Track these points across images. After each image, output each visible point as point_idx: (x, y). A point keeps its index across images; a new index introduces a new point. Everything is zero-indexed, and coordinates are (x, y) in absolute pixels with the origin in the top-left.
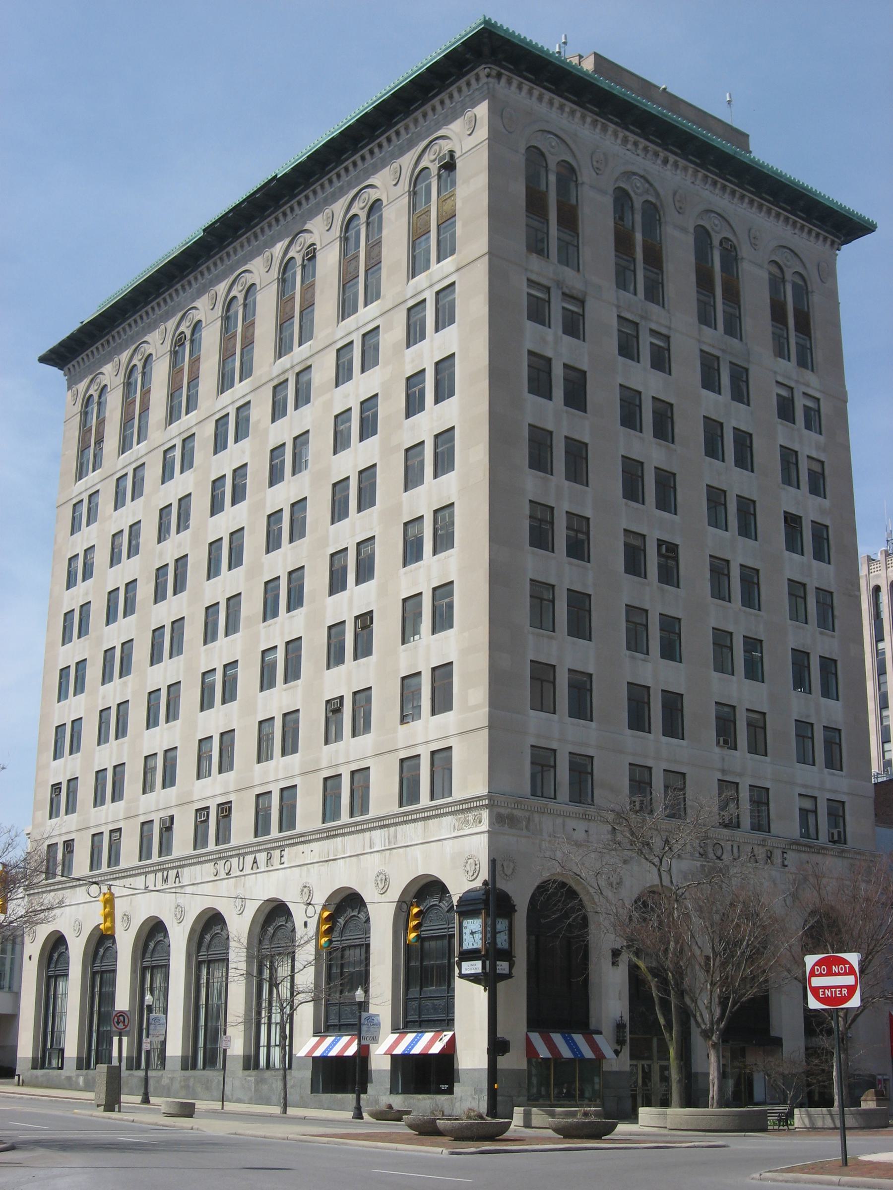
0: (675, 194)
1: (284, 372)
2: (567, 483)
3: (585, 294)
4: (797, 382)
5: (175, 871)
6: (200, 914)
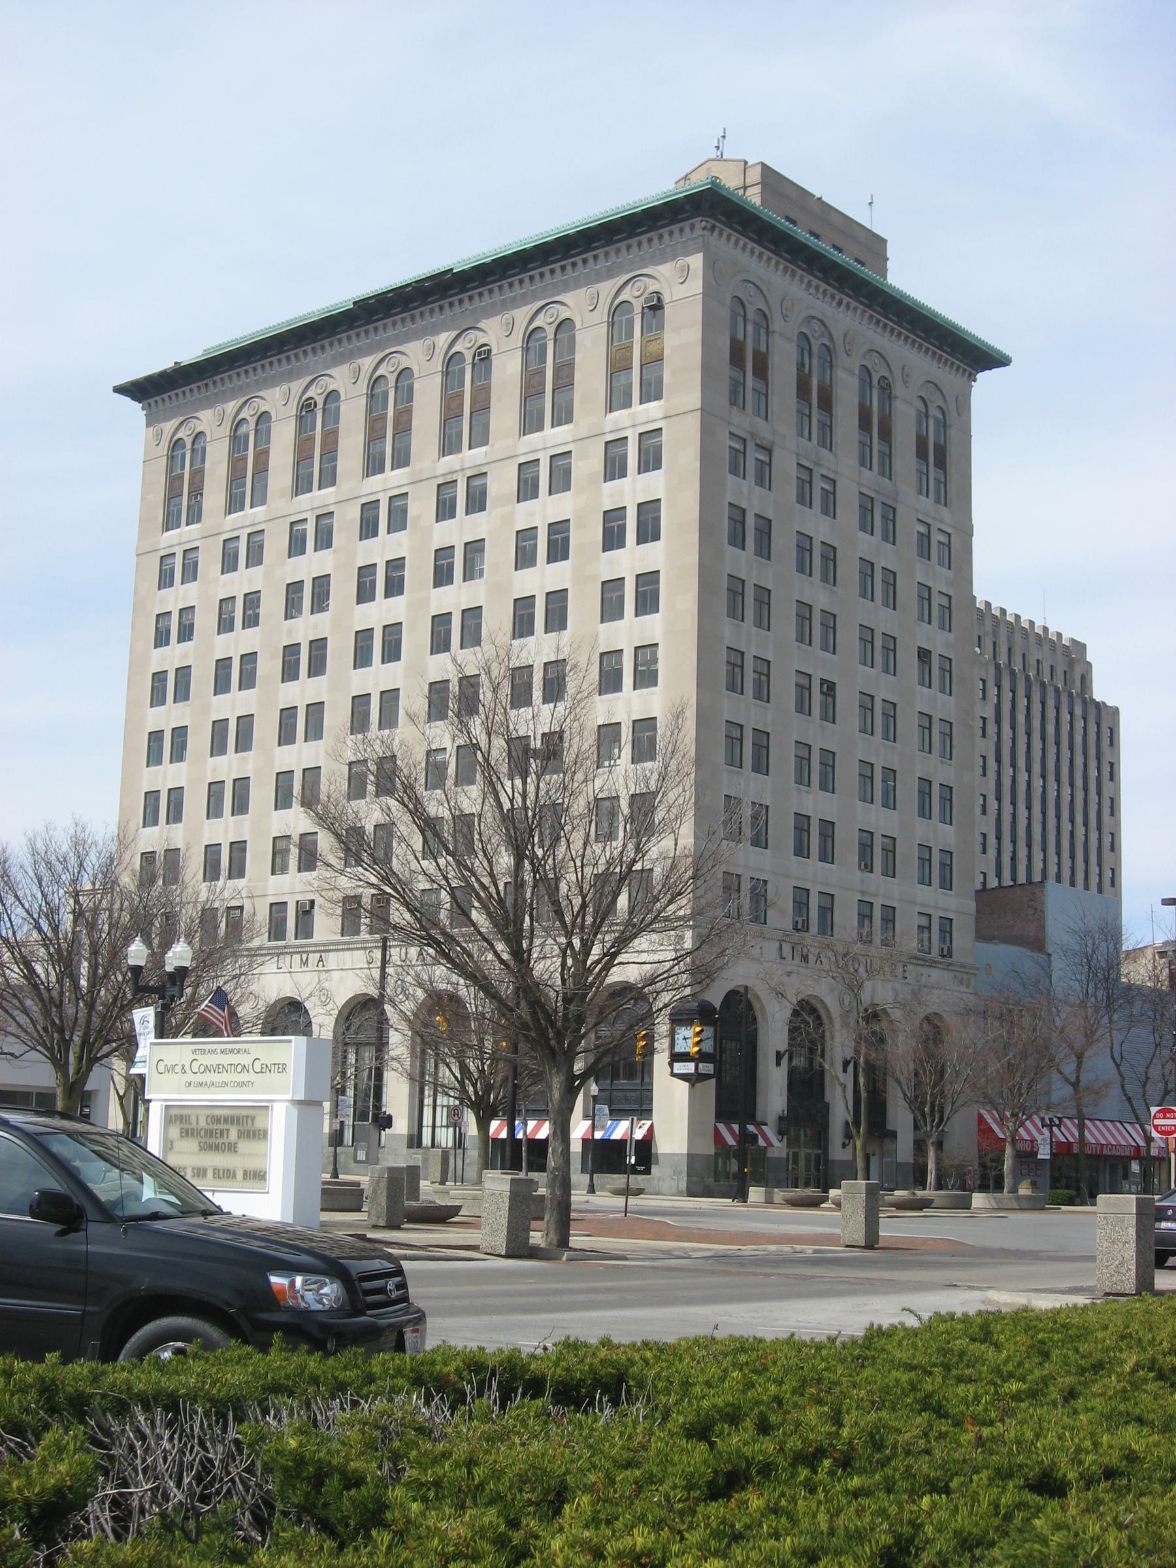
0: (845, 335)
2: (755, 629)
3: (773, 443)
4: (934, 518)
5: (318, 955)
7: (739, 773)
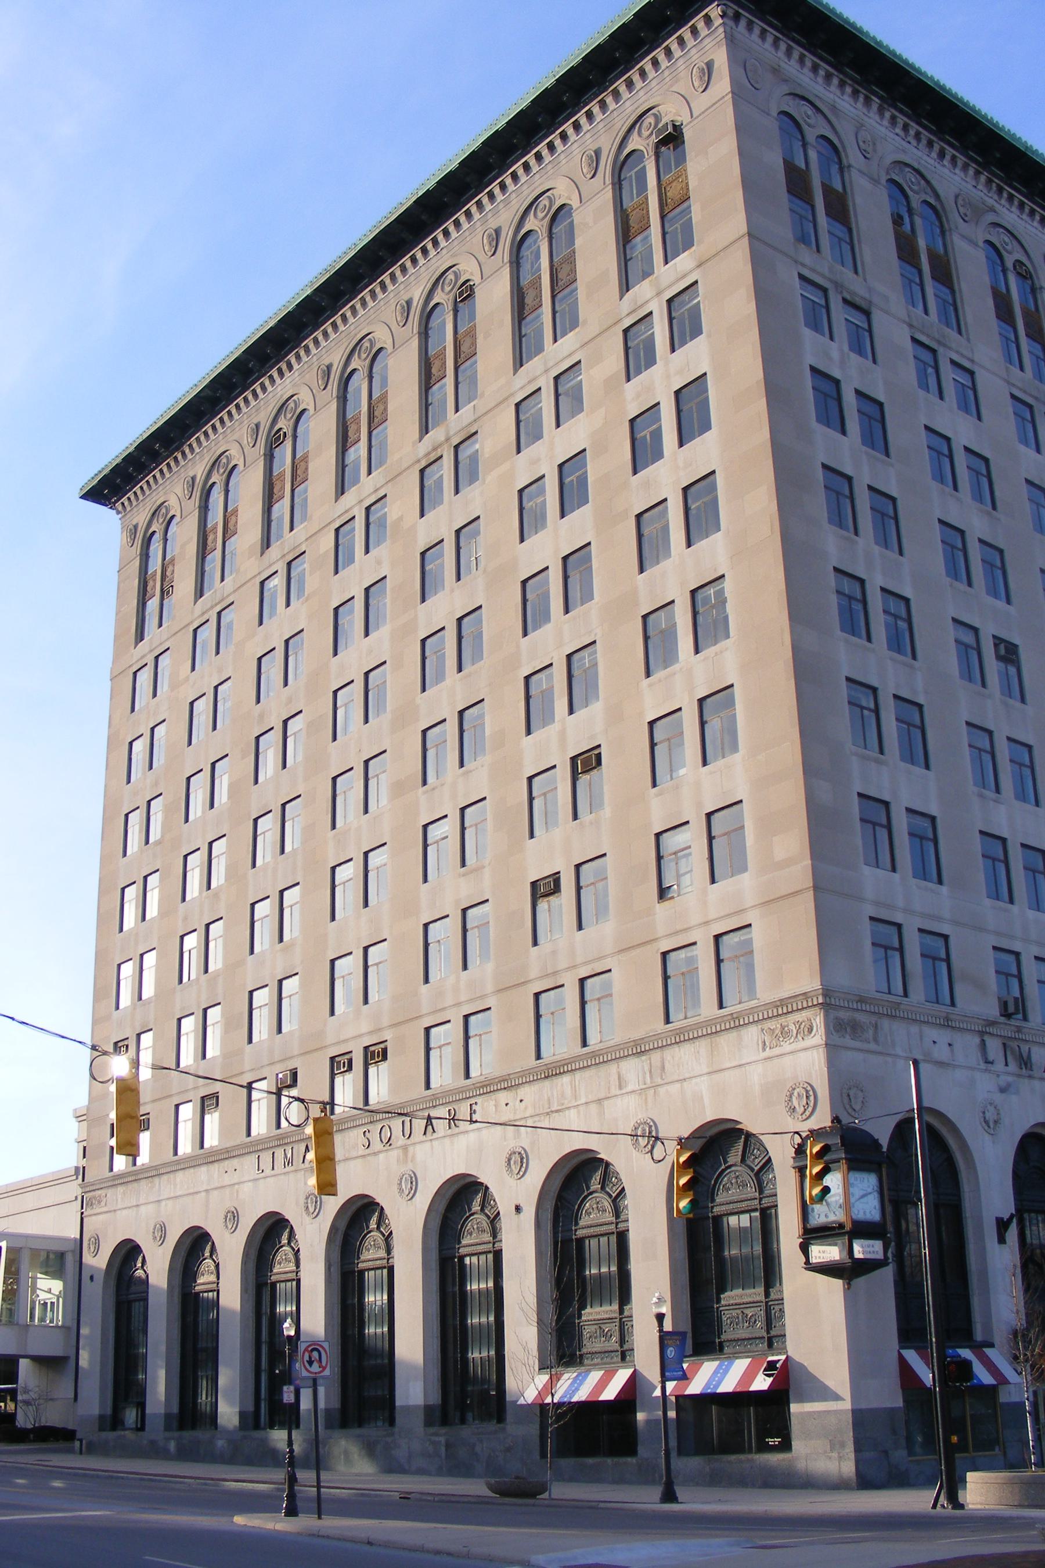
0: (957, 197)
1: (435, 449)
6: (344, 1204)
7: (877, 761)
